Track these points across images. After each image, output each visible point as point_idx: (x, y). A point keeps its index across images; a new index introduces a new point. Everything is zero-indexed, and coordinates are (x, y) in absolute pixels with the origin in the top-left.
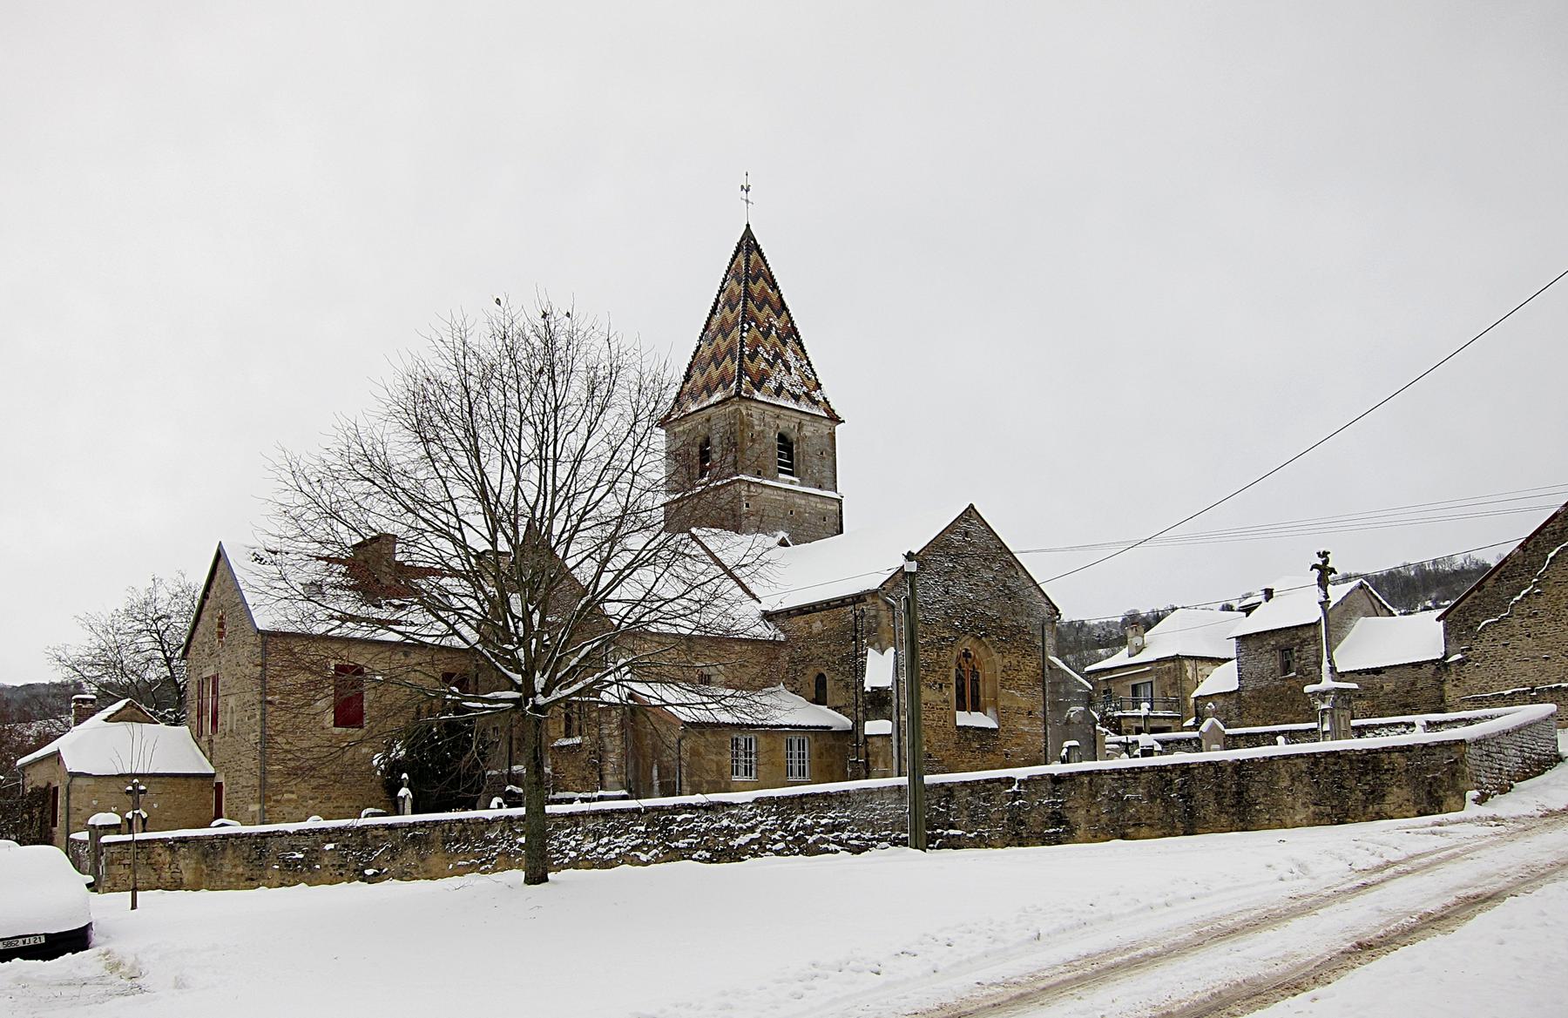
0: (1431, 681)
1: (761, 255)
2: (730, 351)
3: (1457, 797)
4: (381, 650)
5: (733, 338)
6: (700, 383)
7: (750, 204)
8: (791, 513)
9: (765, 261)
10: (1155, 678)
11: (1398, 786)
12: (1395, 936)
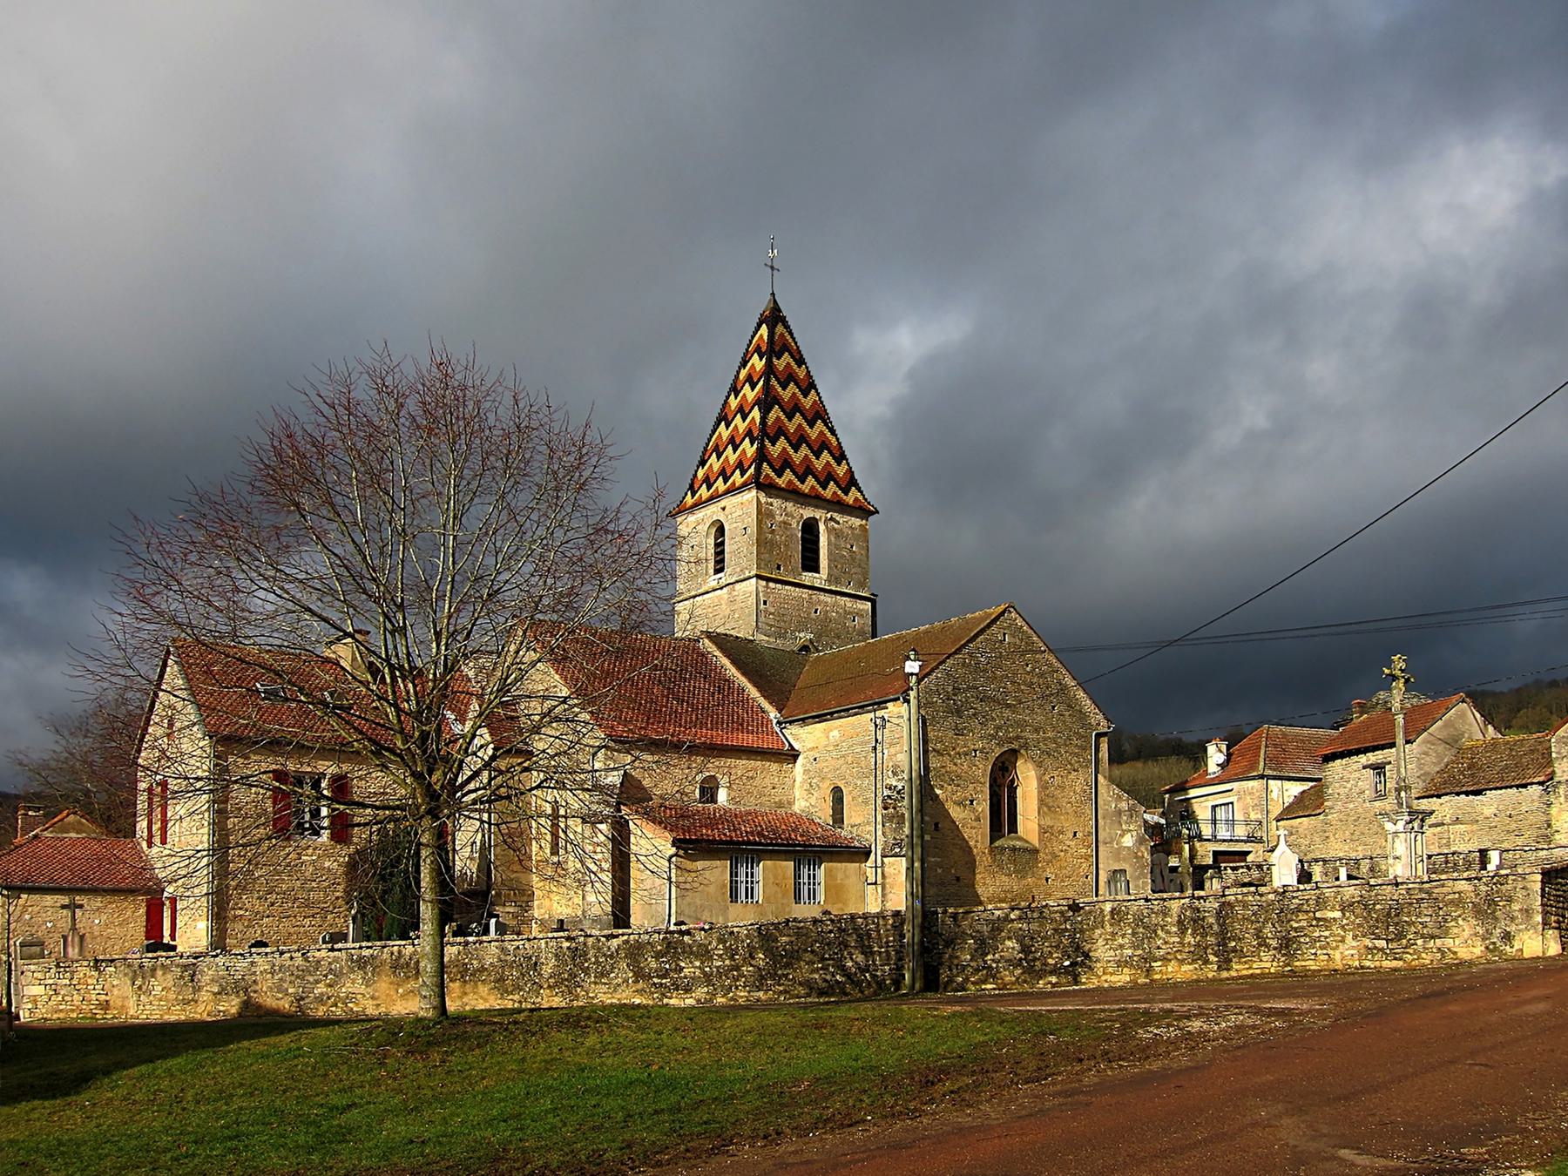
0: (1536, 804)
1: (787, 327)
2: (749, 433)
3: (1531, 931)
4: (30, 1105)
5: (753, 418)
6: (716, 466)
7: (775, 272)
8: (816, 612)
9: (791, 334)
10: (1236, 798)
11: (1464, 919)
12: (695, 929)
